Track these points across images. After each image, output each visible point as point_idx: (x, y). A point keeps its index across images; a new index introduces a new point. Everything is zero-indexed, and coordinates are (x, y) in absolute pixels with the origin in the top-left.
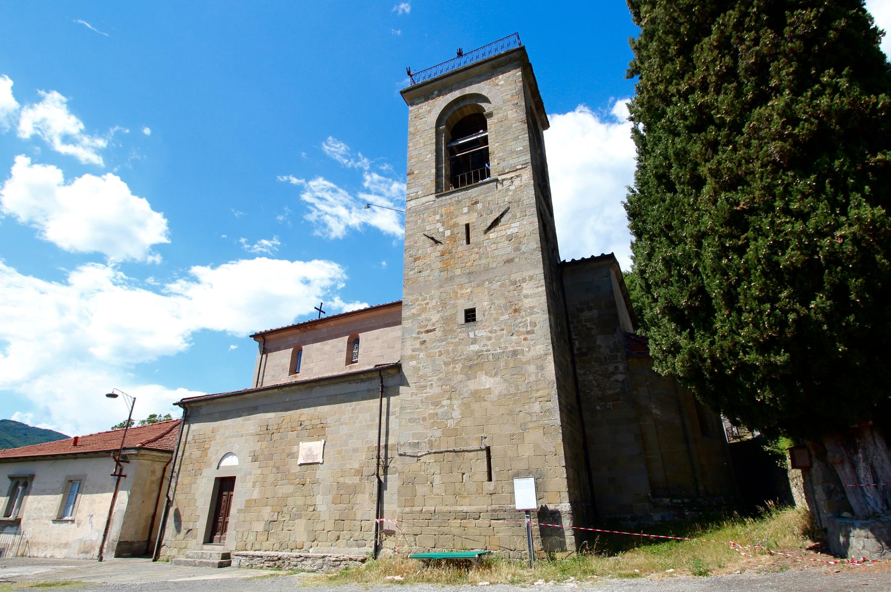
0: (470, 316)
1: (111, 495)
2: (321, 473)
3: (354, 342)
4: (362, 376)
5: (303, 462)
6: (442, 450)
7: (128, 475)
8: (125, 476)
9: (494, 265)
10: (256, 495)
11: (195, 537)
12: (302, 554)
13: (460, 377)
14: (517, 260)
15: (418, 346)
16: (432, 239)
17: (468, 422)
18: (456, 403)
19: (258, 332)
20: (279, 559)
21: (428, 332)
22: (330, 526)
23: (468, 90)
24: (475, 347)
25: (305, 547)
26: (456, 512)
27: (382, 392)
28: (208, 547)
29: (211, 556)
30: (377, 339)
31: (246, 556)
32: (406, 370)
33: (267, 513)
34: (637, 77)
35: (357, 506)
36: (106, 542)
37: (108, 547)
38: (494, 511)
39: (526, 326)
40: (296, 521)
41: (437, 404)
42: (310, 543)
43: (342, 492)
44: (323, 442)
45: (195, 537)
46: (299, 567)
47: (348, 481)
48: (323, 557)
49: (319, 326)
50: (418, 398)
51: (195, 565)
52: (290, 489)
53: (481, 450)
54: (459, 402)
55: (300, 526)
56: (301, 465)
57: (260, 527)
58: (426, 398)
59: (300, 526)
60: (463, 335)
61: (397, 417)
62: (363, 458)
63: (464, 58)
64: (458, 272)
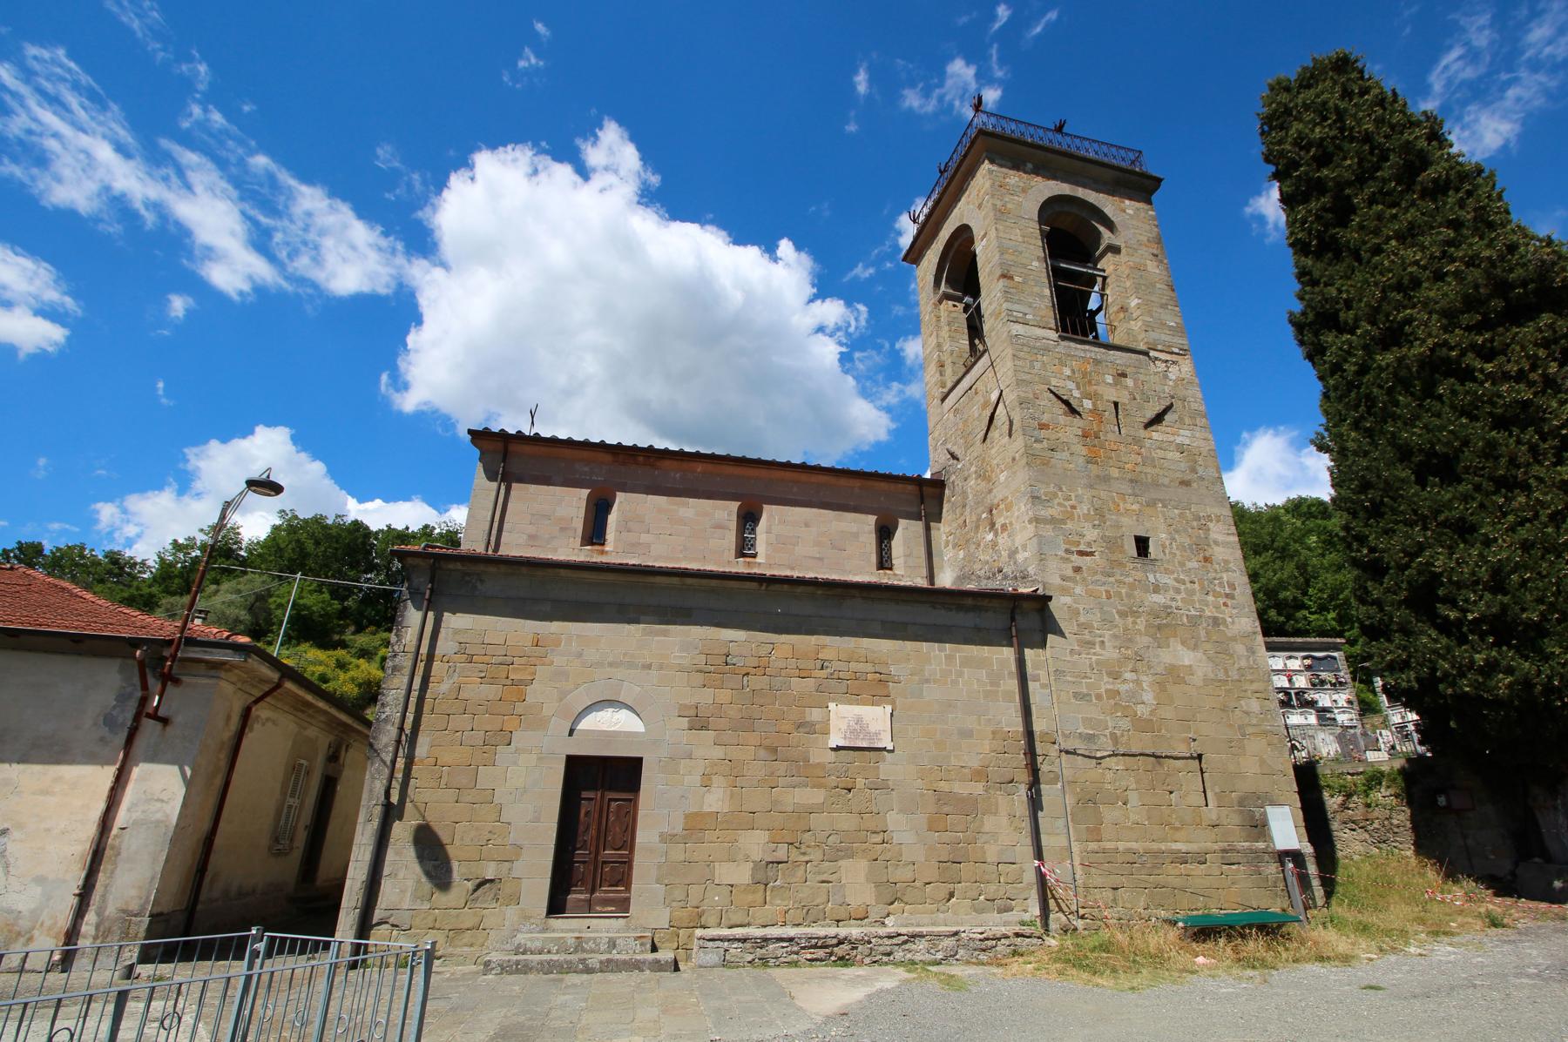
0: (1142, 544)
1: (109, 772)
2: (888, 769)
3: (748, 519)
4: (969, 601)
5: (841, 744)
6: (1134, 750)
7: (178, 719)
8: (165, 721)
9: (1166, 481)
10: (715, 800)
11: (516, 899)
12: (903, 930)
13: (1146, 640)
14: (1195, 485)
15: (1069, 572)
16: (1067, 403)
17: (1167, 713)
18: (1146, 680)
20: (840, 943)
21: (1081, 553)
22: (932, 873)
23: (1081, 193)
24: (1159, 599)
25: (873, 916)
26: (1172, 852)
27: (429, 601)
28: (556, 923)
30: (807, 525)
31: (744, 940)
32: (1057, 607)
33: (755, 844)
35: (984, 838)
36: (91, 917)
37: (102, 932)
38: (1224, 851)
39: (1221, 584)
40: (841, 863)
41: (1116, 676)
43: (946, 809)
44: (889, 708)
45: (516, 899)
47: (961, 789)
48: (956, 933)
49: (667, 463)
50: (1084, 660)
51: (589, 970)
52: (815, 796)
53: (1192, 758)
54: (1150, 678)
56: (838, 748)
57: (742, 874)
58: (1098, 663)
60: (1139, 575)
61: (1043, 686)
63: (1059, 136)
64: (1115, 473)
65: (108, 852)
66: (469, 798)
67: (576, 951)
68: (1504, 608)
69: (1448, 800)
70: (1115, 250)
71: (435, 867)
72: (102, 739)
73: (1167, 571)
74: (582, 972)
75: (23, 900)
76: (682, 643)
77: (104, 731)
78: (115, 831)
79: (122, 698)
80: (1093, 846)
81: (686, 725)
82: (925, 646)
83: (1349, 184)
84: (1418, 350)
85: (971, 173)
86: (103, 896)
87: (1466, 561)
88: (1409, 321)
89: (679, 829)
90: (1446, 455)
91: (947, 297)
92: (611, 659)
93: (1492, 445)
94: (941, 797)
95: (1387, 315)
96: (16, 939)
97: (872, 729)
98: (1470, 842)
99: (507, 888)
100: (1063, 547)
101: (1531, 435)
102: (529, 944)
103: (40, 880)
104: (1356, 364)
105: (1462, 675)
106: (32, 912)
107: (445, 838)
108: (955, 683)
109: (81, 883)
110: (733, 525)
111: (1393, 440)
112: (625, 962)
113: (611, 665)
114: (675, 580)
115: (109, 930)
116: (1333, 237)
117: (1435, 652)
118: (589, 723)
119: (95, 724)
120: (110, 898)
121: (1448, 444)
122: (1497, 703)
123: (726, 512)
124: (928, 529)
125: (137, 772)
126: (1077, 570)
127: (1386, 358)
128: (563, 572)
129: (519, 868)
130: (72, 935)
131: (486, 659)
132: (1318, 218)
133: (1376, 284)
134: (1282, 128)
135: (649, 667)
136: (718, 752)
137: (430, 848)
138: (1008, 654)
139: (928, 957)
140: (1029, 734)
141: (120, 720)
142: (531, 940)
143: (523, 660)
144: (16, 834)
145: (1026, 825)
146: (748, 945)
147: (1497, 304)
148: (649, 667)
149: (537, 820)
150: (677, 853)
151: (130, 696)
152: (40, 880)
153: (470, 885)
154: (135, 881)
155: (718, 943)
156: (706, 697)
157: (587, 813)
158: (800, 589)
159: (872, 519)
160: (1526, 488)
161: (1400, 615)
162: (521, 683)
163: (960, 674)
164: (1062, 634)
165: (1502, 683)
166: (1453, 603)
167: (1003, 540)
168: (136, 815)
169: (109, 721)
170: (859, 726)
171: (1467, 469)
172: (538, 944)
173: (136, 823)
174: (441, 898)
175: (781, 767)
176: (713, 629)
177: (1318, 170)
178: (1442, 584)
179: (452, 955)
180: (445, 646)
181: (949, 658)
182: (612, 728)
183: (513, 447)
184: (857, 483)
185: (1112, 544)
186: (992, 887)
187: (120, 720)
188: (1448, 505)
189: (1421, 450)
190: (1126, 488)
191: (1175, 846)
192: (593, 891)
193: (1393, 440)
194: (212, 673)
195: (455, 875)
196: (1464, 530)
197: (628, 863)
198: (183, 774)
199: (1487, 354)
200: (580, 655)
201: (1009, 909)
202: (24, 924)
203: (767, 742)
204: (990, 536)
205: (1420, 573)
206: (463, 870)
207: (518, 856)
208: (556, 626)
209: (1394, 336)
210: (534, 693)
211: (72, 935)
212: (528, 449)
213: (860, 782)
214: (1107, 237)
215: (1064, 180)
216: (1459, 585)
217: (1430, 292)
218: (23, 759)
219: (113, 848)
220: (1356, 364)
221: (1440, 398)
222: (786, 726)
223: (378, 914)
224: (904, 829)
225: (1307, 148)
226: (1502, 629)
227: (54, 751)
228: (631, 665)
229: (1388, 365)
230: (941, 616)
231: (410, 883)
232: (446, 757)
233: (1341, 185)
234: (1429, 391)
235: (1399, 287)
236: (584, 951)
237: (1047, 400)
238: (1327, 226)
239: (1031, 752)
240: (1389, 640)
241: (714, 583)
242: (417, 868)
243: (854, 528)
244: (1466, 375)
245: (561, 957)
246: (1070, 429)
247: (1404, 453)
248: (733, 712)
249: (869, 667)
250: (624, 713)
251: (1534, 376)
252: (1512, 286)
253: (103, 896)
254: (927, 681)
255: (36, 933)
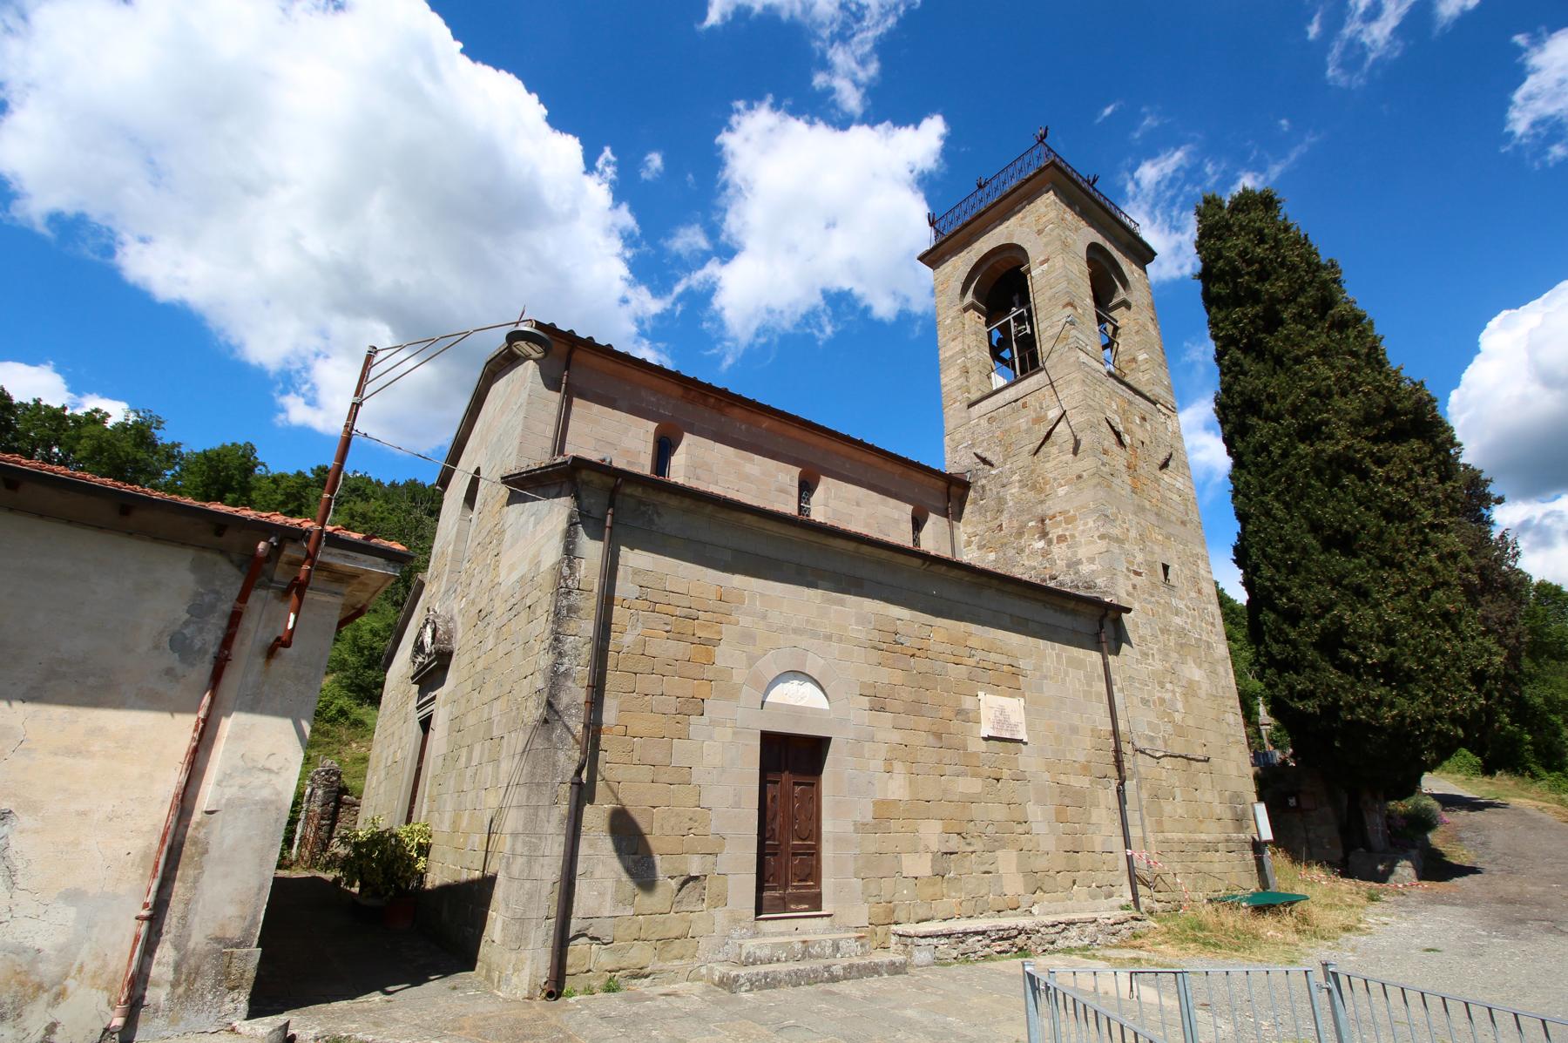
2: (1028, 760)
10: (897, 788)
11: (721, 900)
19: (563, 326)
23: (1117, 255)
31: (948, 936)
37: (186, 975)
40: (999, 853)
42: (1029, 898)
43: (1067, 801)
45: (721, 900)
46: (1060, 943)
49: (737, 412)
55: (1007, 861)
57: (919, 865)
59: (1007, 861)
62: (1088, 746)
64: (1147, 505)
65: (187, 849)
66: (666, 778)
67: (803, 957)
68: (1392, 656)
70: (1126, 304)
71: (636, 863)
72: (169, 672)
73: (1182, 599)
75: (45, 930)
76: (859, 615)
77: (172, 659)
78: (197, 816)
79: (198, 611)
80: (1160, 836)
81: (867, 706)
83: (1280, 301)
85: (1031, 197)
88: (1326, 423)
89: (869, 818)
90: (1347, 533)
91: (972, 306)
92: (794, 625)
93: (1381, 532)
94: (1064, 790)
96: (34, 998)
97: (1013, 721)
98: (1311, 835)
101: (1405, 527)
102: (758, 953)
103: (73, 896)
106: (62, 949)
108: (1064, 681)
111: (1307, 515)
112: (865, 967)
113: (795, 631)
115: (197, 971)
116: (1260, 341)
119: (156, 647)
120: (195, 921)
122: (1382, 729)
123: (789, 476)
124: (951, 527)
126: (1134, 587)
127: (1303, 448)
129: (724, 862)
130: (139, 981)
131: (669, 609)
132: (1252, 322)
135: (829, 638)
136: (896, 737)
137: (629, 837)
138: (1095, 657)
140: (1115, 733)
141: (198, 644)
142: (760, 947)
143: (709, 616)
144: (24, 820)
145: (1117, 816)
146: (952, 940)
147: (1389, 424)
148: (829, 638)
149: (737, 805)
151: (212, 608)
152: (73, 896)
153: (674, 884)
154: (229, 897)
155: (929, 940)
156: (886, 676)
159: (909, 508)
160: (1400, 567)
161: (1311, 654)
163: (1066, 674)
165: (1387, 715)
166: (1354, 649)
167: (1059, 551)
168: (231, 792)
169: (179, 644)
171: (1363, 546)
173: (230, 804)
174: (645, 901)
175: (948, 755)
176: (882, 604)
178: (1347, 634)
179: (662, 971)
180: (625, 587)
182: (799, 703)
184: (898, 469)
186: (1100, 875)
187: (198, 644)
188: (1350, 573)
189: (1331, 527)
190: (1153, 518)
191: (1203, 837)
193: (1307, 515)
194: (334, 587)
196: (1361, 593)
197: (814, 853)
198: (300, 732)
201: (1110, 895)
202: (48, 970)
203: (935, 728)
204: (1041, 544)
207: (722, 846)
208: (738, 581)
209: (1310, 432)
210: (726, 655)
211: (139, 981)
212: (595, 361)
213: (1006, 773)
214: (1121, 294)
216: (1362, 636)
217: (1339, 402)
218: (34, 694)
219: (195, 843)
221: (1342, 488)
222: (949, 714)
225: (1249, 263)
226: (1390, 673)
227: (95, 687)
228: (814, 635)
231: (610, 884)
232: (637, 726)
233: (1274, 300)
234: (1335, 481)
235: (1316, 394)
236: (811, 956)
237: (1105, 428)
238: (1257, 330)
239: (1118, 751)
240: (1298, 674)
241: (884, 554)
242: (616, 864)
244: (1363, 475)
245: (793, 966)
246: (1119, 458)
247: (1315, 527)
250: (809, 687)
251: (1408, 484)
254: (1045, 677)
255: (71, 983)
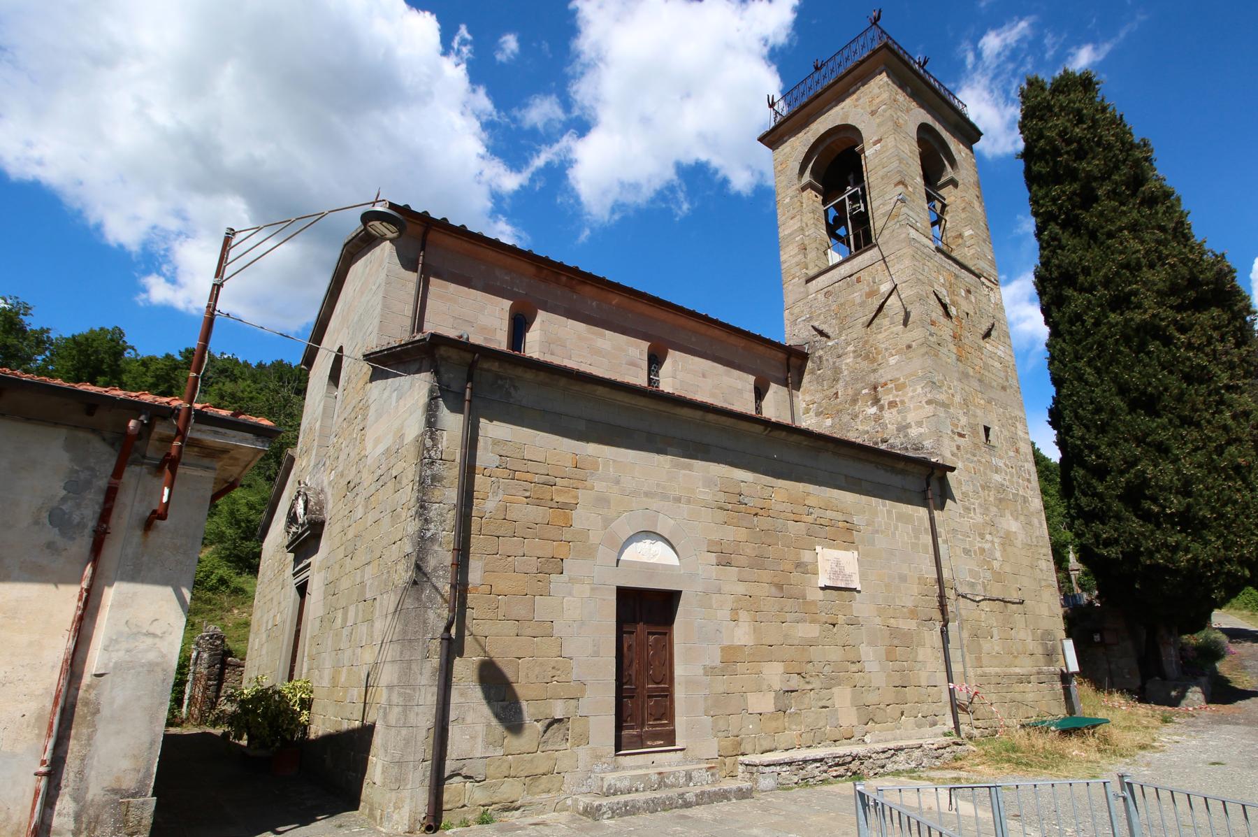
2: (861, 607)
10: (742, 635)
11: (583, 739)
17: (1007, 569)
19: (417, 207)
22: (890, 696)
29: (689, 777)
30: (704, 376)
31: (790, 764)
34: (937, 227)
36: (65, 804)
40: (834, 690)
43: (896, 642)
45: (583, 739)
46: (890, 767)
49: (588, 290)
51: (687, 805)
52: (809, 630)
55: (842, 697)
57: (764, 703)
59: (842, 697)
62: (915, 592)
64: (971, 372)
65: (80, 710)
66: (529, 631)
68: (1189, 506)
69: (1102, 637)
70: (954, 183)
71: (504, 708)
72: (50, 546)
73: (1001, 458)
74: (682, 807)
76: (706, 477)
77: (53, 534)
78: (87, 679)
79: (75, 488)
80: (979, 671)
82: (874, 501)
83: (1095, 179)
84: (1138, 317)
85: (865, 79)
86: (80, 773)
87: (1164, 473)
89: (717, 662)
90: (1151, 395)
94: (894, 632)
95: (1118, 286)
98: (1113, 666)
99: (574, 727)
100: (950, 427)
101: (1203, 389)
102: (618, 784)
104: (1093, 317)
105: (1158, 551)
107: (509, 673)
109: (47, 756)
110: (645, 364)
111: (1115, 379)
112: (715, 793)
113: (647, 494)
114: (698, 414)
116: (1077, 216)
117: (1142, 534)
118: (631, 554)
119: (36, 523)
120: (92, 775)
121: (1156, 388)
122: (1178, 571)
124: (791, 396)
125: (111, 594)
126: (958, 448)
128: (601, 390)
129: (585, 705)
132: (1069, 199)
133: (1113, 261)
134: (1041, 119)
136: (741, 589)
138: (922, 512)
139: (907, 767)
141: (76, 518)
142: (620, 779)
143: (565, 482)
145: (941, 655)
146: (794, 768)
147: (1192, 294)
149: (596, 654)
150: (720, 684)
151: (88, 484)
153: (540, 726)
156: (731, 534)
157: (630, 646)
158: (795, 438)
159: (752, 379)
160: (1198, 425)
161: (1116, 506)
162: (563, 507)
164: (954, 500)
165: (1183, 559)
166: (1154, 500)
169: (58, 519)
170: (838, 571)
172: (626, 783)
173: (118, 667)
174: (513, 742)
177: (1075, 161)
179: (531, 804)
181: (889, 512)
182: (651, 560)
183: (434, 236)
184: (742, 343)
185: (973, 428)
187: (76, 518)
188: (1153, 431)
189: (1137, 389)
191: (1018, 670)
192: (643, 725)
193: (1115, 379)
194: (206, 462)
195: (527, 719)
196: (1163, 449)
197: (668, 695)
199: (1183, 329)
200: (617, 482)
201: (934, 724)
203: (776, 580)
204: (874, 410)
205: (1136, 476)
206: (532, 710)
207: (583, 691)
208: (592, 449)
209: (1121, 302)
210: (582, 518)
212: (449, 241)
213: (841, 619)
215: (934, 116)
216: (1162, 489)
219: (87, 703)
220: (1093, 317)
221: (1149, 353)
222: (788, 566)
223: (449, 766)
224: (870, 655)
226: (1186, 521)
228: (664, 497)
229: (1117, 323)
230: (882, 476)
231: (480, 729)
232: (500, 586)
233: (1090, 177)
234: (1142, 347)
236: (666, 786)
237: (933, 301)
238: (1074, 207)
242: (486, 710)
243: (739, 385)
244: (1167, 341)
245: (649, 795)
247: (1123, 390)
248: (749, 550)
249: (840, 517)
251: (1207, 350)
252: (1201, 284)
253: (80, 773)
254: (877, 532)
